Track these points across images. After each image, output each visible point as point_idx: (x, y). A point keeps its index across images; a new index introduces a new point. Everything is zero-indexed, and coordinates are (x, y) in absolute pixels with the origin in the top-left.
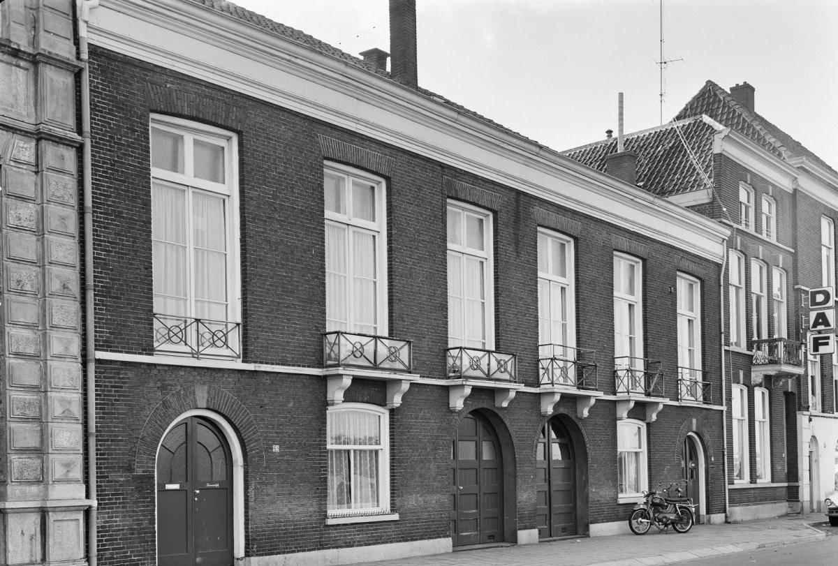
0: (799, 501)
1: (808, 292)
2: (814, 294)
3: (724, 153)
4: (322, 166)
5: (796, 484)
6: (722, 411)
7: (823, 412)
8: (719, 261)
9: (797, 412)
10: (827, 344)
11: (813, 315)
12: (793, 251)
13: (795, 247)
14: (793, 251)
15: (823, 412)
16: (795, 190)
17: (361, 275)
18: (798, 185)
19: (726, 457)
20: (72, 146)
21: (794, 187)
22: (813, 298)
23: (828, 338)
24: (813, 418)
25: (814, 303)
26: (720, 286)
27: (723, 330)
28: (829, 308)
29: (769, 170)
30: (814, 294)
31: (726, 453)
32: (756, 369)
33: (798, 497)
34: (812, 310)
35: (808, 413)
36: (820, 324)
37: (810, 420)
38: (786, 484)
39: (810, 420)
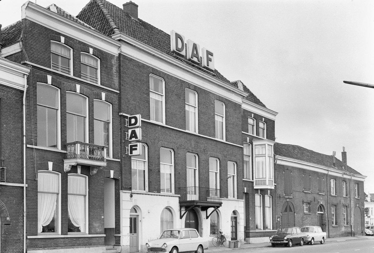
0: (120, 246)
1: (128, 117)
2: (130, 118)
3: (27, 18)
4: (50, 43)
5: (118, 235)
6: (23, 187)
7: (149, 191)
8: (21, 89)
9: (121, 191)
10: (136, 149)
11: (130, 131)
12: (118, 92)
13: (120, 90)
14: (118, 92)
15: (149, 191)
16: (120, 54)
17: (157, 120)
18: (121, 52)
19: (25, 218)
20: (93, 48)
21: (119, 52)
22: (130, 121)
23: (136, 146)
24: (134, 195)
25: (130, 124)
26: (23, 105)
27: (24, 134)
28: (137, 127)
29: (363, 82)
30: (130, 118)
31: (25, 215)
32: (67, 162)
33: (120, 243)
34: (130, 128)
35: (130, 192)
36: (133, 137)
37: (131, 196)
38: (105, 235)
39: (131, 196)
